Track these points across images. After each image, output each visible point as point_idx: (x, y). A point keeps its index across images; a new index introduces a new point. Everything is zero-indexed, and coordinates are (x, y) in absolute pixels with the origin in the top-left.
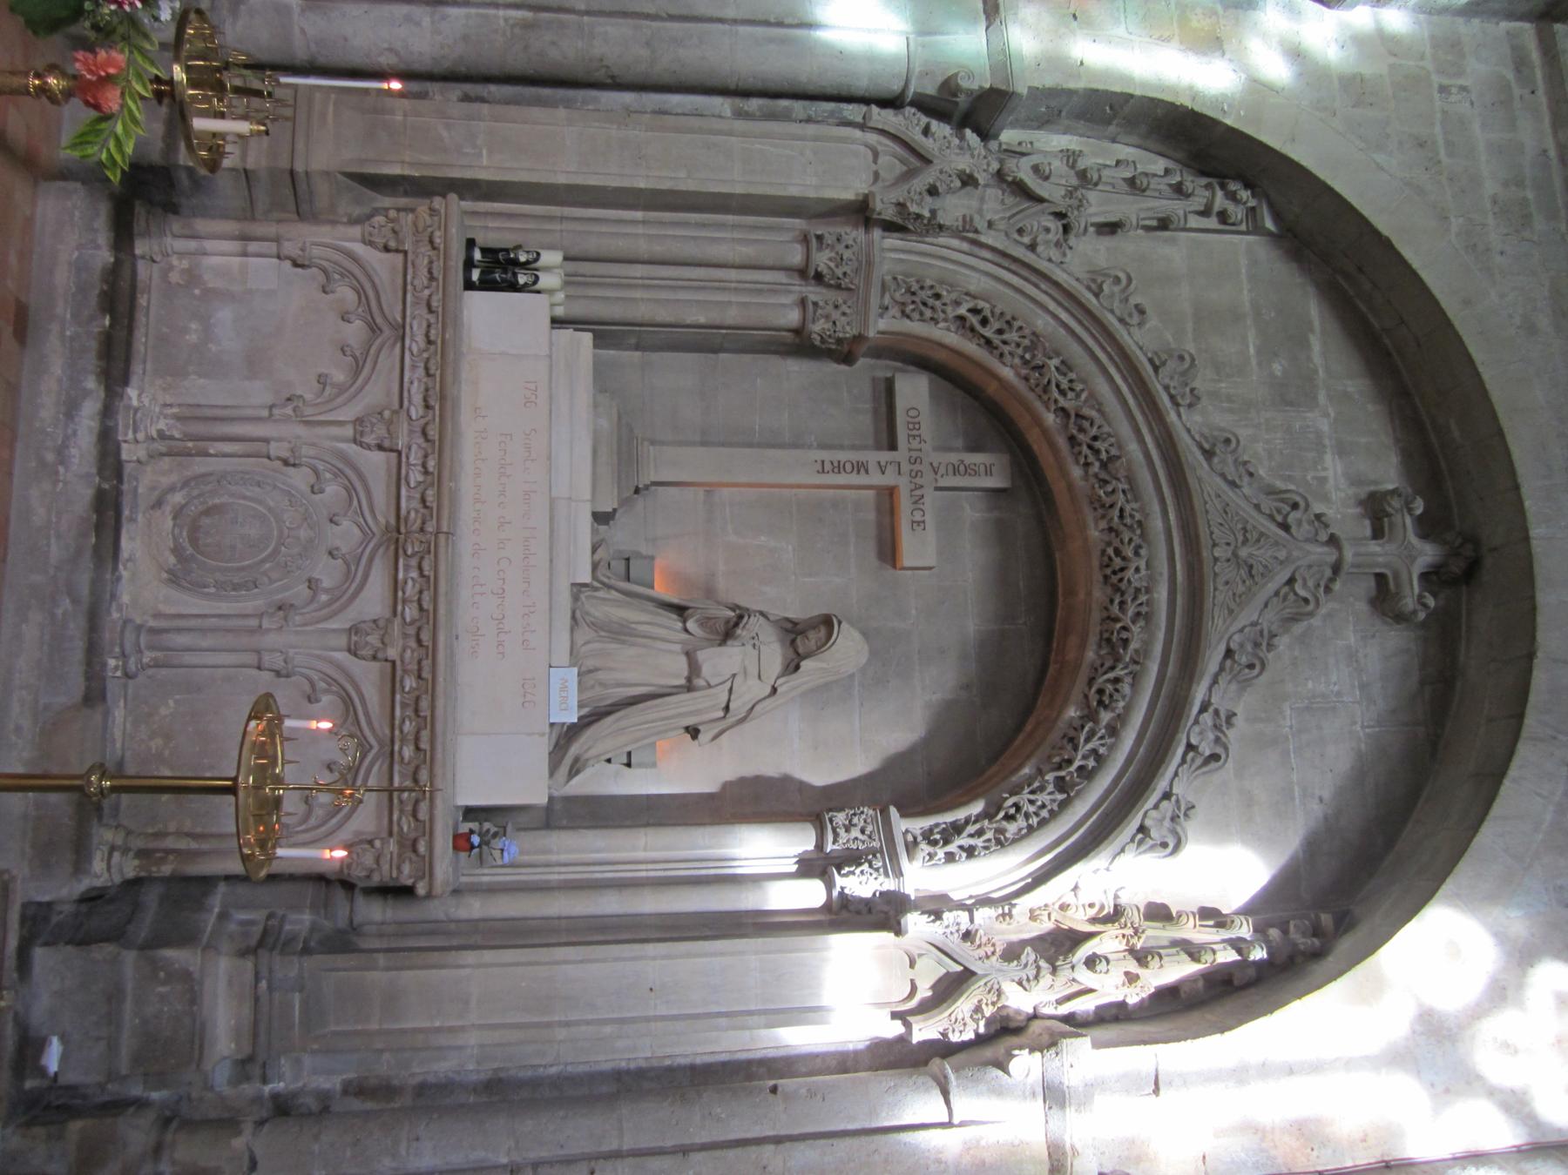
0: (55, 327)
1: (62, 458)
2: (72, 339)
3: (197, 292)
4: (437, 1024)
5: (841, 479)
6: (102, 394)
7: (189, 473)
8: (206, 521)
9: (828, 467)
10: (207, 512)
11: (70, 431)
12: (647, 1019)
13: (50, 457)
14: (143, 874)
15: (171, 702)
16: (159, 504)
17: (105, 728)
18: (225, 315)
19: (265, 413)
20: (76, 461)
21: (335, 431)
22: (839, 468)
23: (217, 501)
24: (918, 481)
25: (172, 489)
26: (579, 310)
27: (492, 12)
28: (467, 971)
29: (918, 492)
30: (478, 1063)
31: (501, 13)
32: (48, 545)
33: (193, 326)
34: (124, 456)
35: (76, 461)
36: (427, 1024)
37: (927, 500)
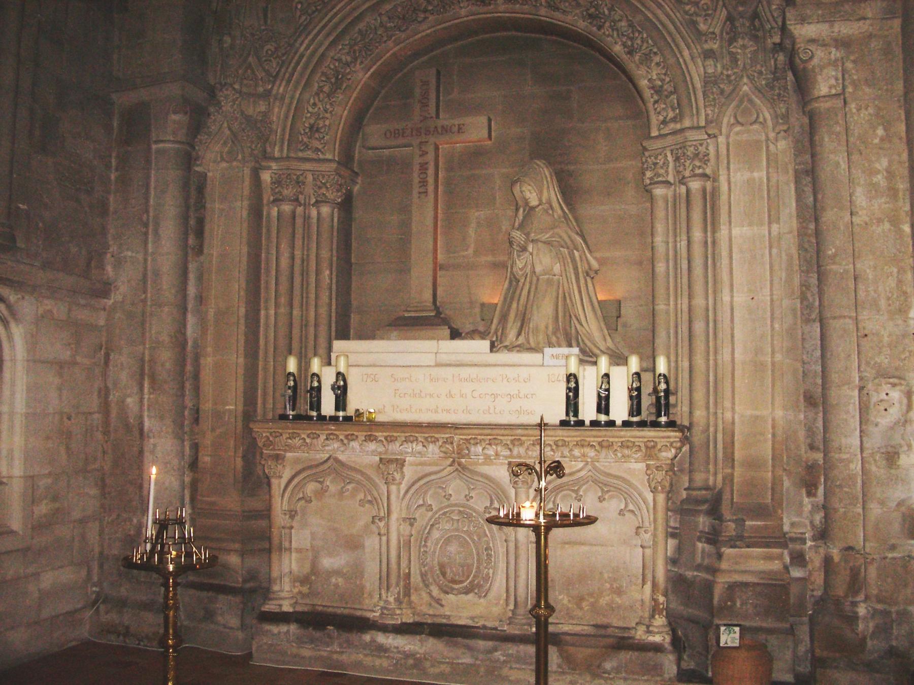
0: (335, 656)
1: (408, 655)
2: (341, 647)
3: (313, 578)
4: (770, 436)
5: (431, 180)
6: (373, 632)
7: (421, 585)
8: (449, 574)
9: (422, 190)
10: (444, 574)
11: (395, 650)
12: (772, 301)
13: (411, 662)
14: (664, 613)
15: (560, 597)
16: (438, 601)
17: (575, 635)
18: (327, 563)
19: (384, 538)
20: (412, 647)
21: (393, 497)
22: (424, 183)
23: (437, 568)
24: (432, 130)
25: (430, 594)
26: (322, 351)
27: (146, 402)
28: (736, 417)
29: (440, 130)
30: (800, 411)
31: (146, 396)
32: (462, 664)
33: (334, 580)
34: (411, 621)
35: (412, 647)
36: (770, 443)
37: (446, 123)
